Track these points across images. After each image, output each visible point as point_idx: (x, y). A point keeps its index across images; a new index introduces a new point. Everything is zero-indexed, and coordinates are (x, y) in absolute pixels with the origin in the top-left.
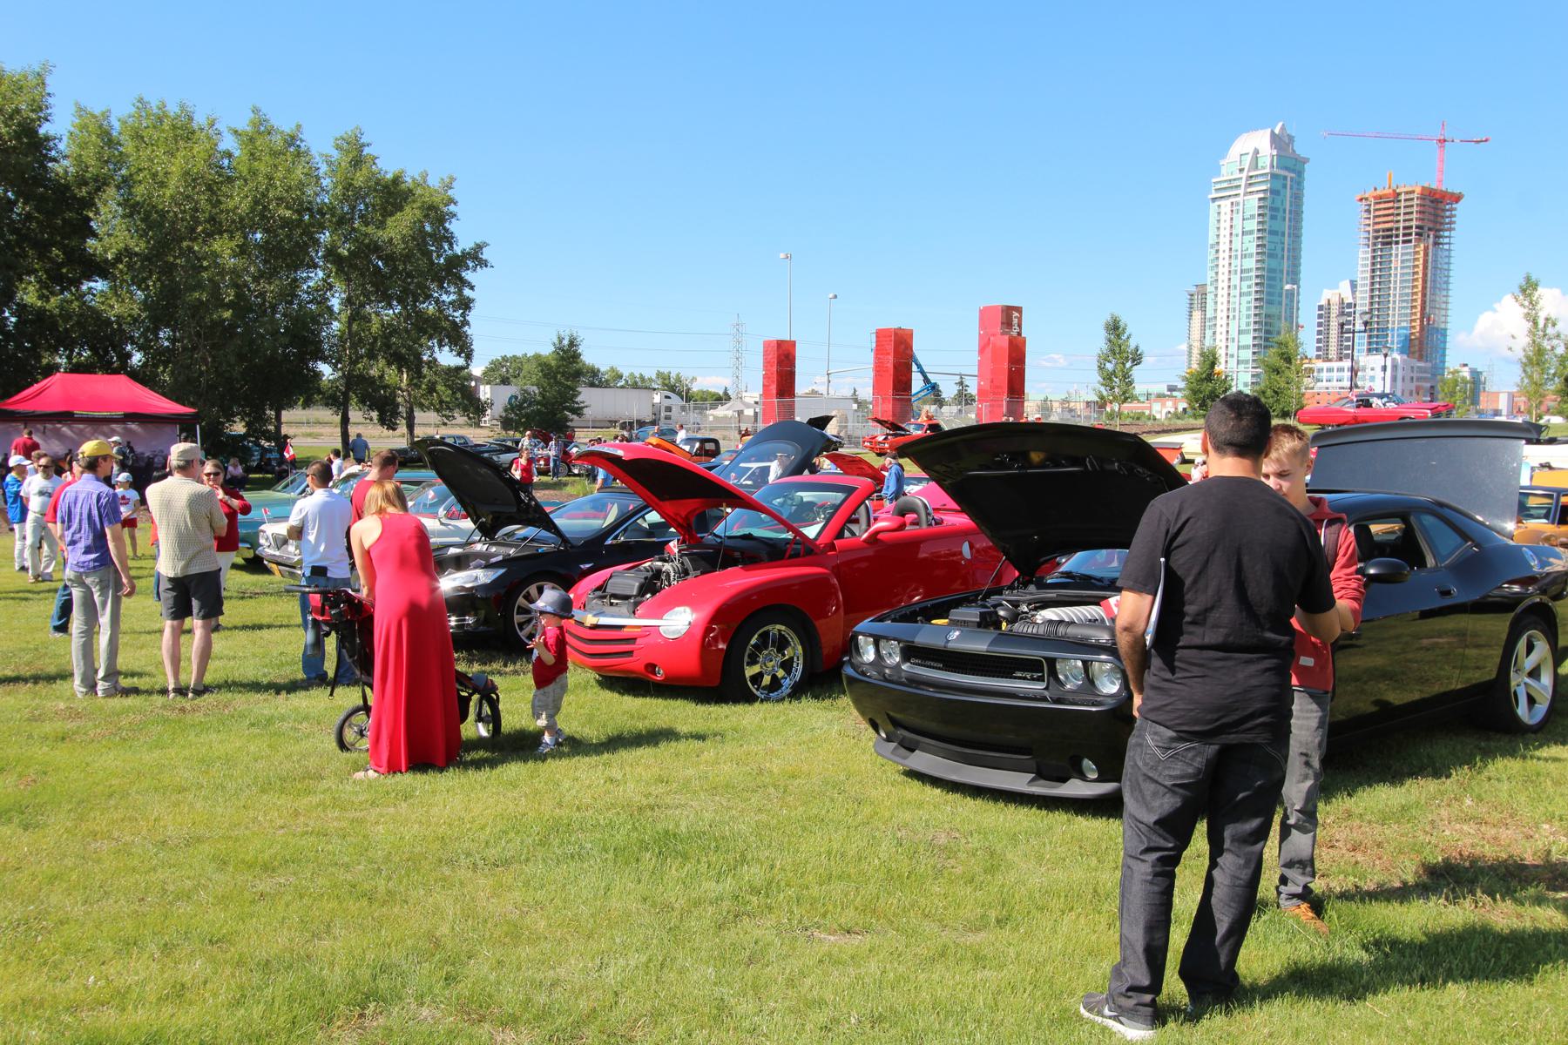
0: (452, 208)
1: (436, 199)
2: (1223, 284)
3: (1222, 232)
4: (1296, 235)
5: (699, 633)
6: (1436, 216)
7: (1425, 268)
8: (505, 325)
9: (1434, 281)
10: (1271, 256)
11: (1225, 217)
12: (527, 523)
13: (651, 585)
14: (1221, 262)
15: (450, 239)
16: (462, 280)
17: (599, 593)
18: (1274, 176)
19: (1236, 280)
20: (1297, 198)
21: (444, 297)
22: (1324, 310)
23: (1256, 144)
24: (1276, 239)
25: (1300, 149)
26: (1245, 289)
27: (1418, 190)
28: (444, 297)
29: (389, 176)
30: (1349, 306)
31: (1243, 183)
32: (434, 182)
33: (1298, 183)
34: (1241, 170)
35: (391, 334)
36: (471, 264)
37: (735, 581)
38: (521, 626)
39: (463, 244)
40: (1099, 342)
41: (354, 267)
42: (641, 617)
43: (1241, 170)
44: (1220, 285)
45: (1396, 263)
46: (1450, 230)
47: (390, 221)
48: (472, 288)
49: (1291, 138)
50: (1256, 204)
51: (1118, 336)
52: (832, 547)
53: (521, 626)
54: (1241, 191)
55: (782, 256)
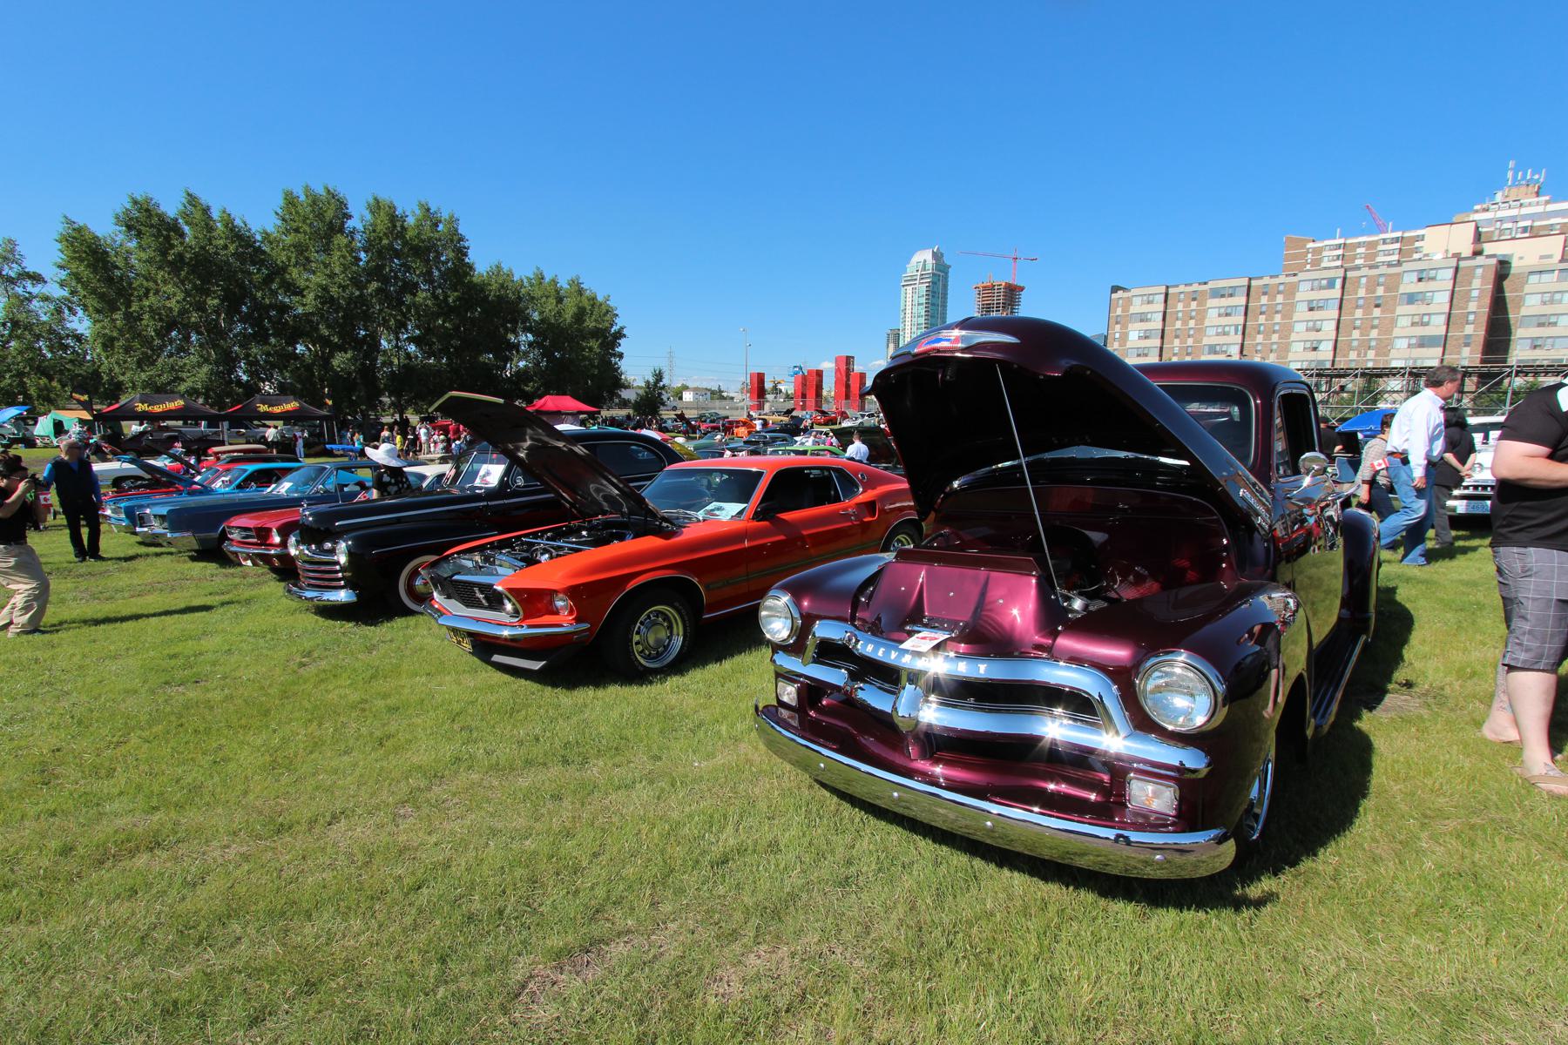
4: (944, 306)
20: (945, 287)
23: (925, 257)
33: (946, 278)
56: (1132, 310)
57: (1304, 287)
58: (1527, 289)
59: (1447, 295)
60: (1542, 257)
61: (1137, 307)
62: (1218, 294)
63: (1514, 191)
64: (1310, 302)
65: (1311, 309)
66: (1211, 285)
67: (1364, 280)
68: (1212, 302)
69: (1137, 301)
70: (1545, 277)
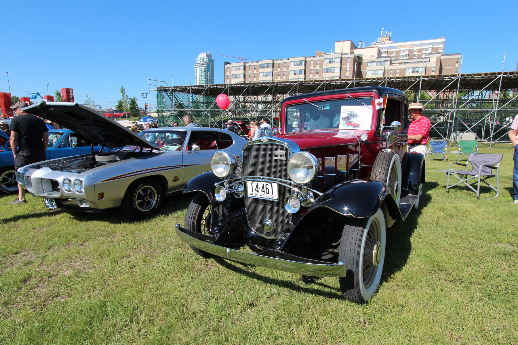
8: (20, 98)
11: (198, 72)
20: (213, 69)
25: (213, 58)
33: (213, 65)
57: (292, 64)
58: (368, 68)
59: (339, 69)
60: (372, 56)
61: (234, 72)
62: (263, 66)
63: (383, 38)
64: (294, 71)
65: (295, 74)
66: (260, 62)
67: (312, 62)
68: (261, 70)
69: (234, 69)
70: (373, 64)
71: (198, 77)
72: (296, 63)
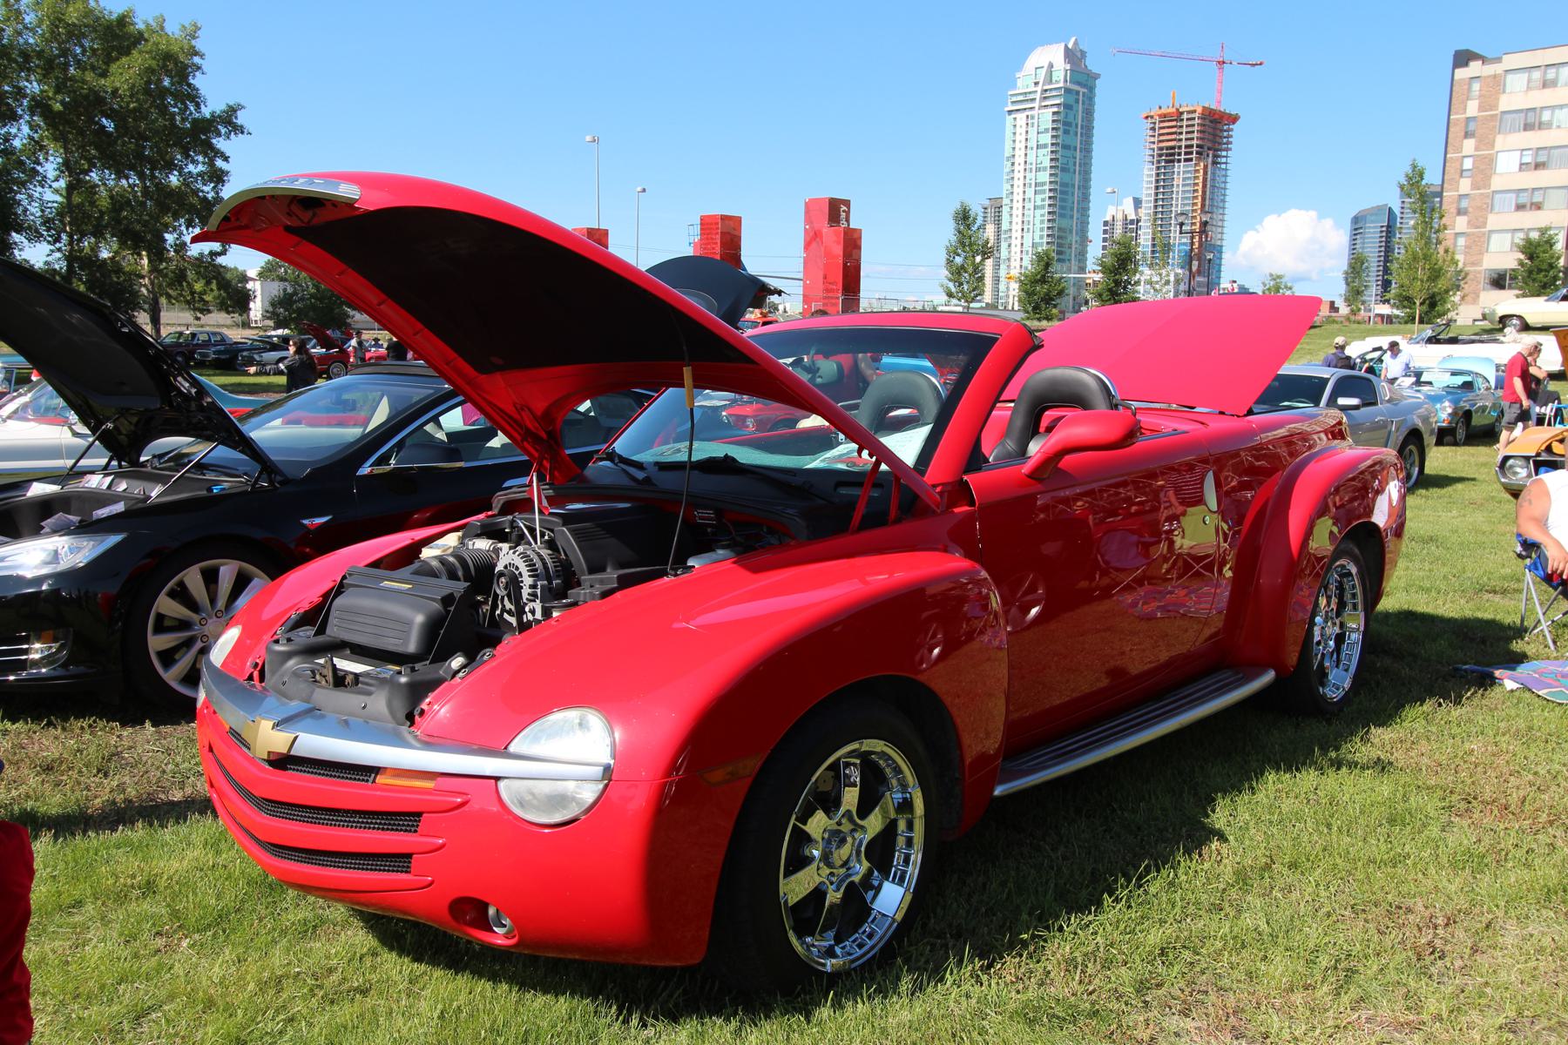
0: (196, 60)
1: (176, 49)
2: (1018, 197)
3: (1018, 145)
4: (1087, 150)
5: (639, 800)
6: (1215, 136)
7: (1204, 186)
9: (1212, 199)
10: (1063, 170)
11: (1021, 130)
12: (200, 433)
13: (468, 622)
14: (1016, 175)
15: (194, 97)
16: (211, 147)
17: (306, 635)
18: (1067, 91)
19: (1030, 192)
20: (1089, 113)
21: (191, 168)
22: (1108, 225)
23: (1051, 57)
24: (1069, 153)
25: (1092, 64)
26: (1039, 203)
27: (1199, 110)
28: (191, 168)
29: (114, 17)
30: (1132, 222)
31: (1038, 96)
32: (173, 29)
34: (1036, 84)
35: (122, 209)
36: (223, 131)
37: (736, 612)
38: (168, 657)
39: (213, 105)
40: (947, 233)
41: (68, 122)
42: (432, 742)
43: (1036, 84)
44: (1015, 197)
45: (1178, 181)
46: (1227, 150)
47: (114, 68)
48: (226, 159)
49: (1083, 54)
50: (1050, 117)
51: (968, 227)
52: (960, 491)
53: (168, 657)
54: (1036, 105)
55: (588, 138)
56: (1505, 103)
69: (1516, 83)
71: (1020, 153)
72: (1536, 75)
